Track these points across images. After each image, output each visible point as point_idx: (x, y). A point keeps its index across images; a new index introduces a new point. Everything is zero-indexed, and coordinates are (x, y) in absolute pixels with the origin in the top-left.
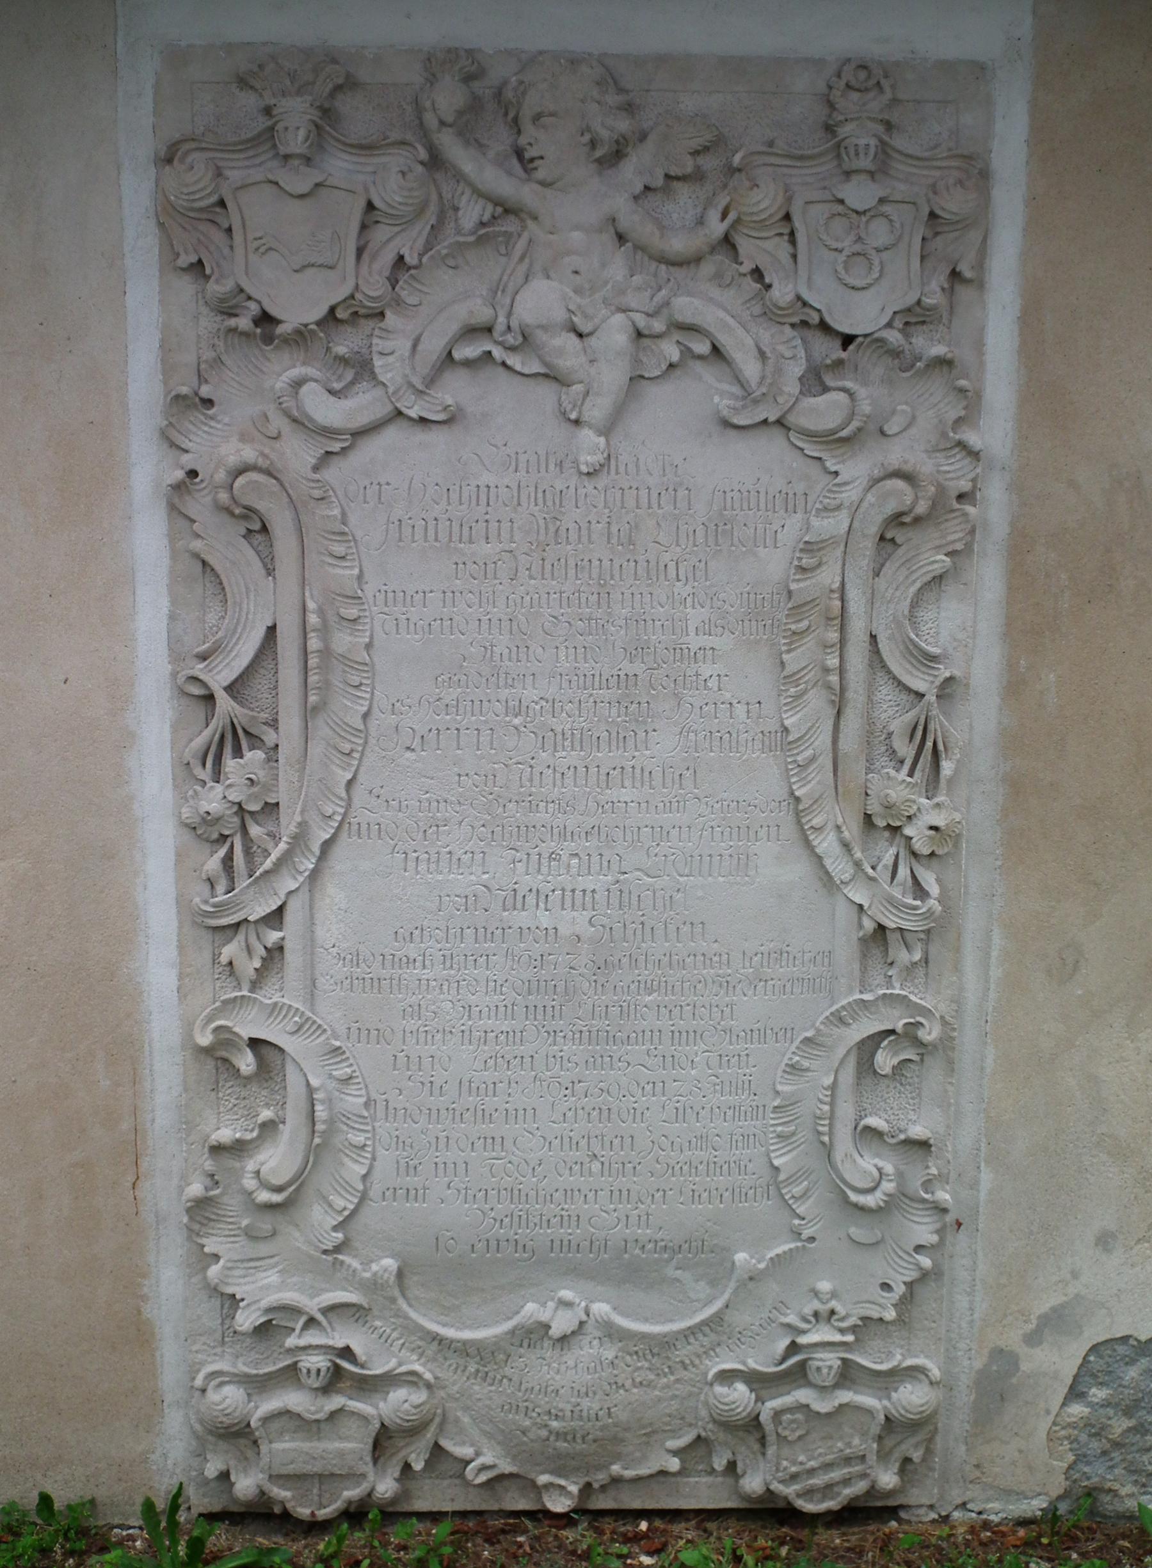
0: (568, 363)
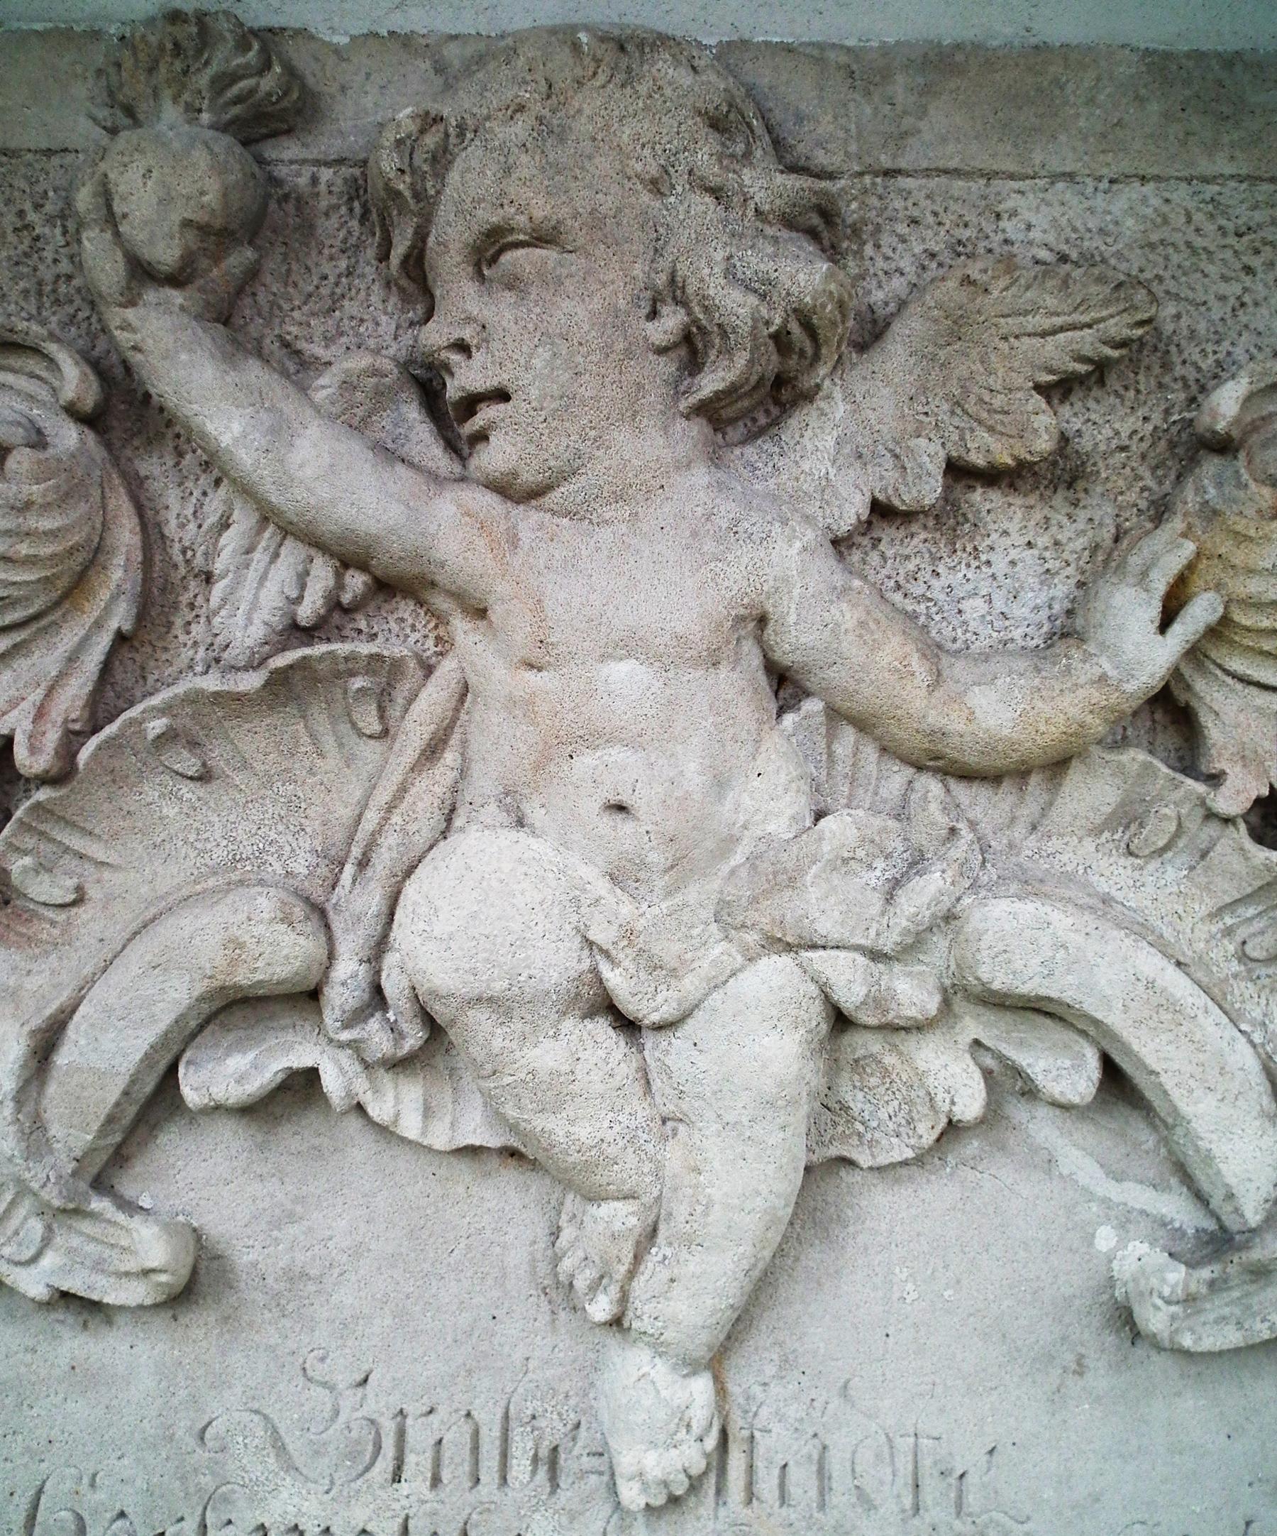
0: (583, 1132)
